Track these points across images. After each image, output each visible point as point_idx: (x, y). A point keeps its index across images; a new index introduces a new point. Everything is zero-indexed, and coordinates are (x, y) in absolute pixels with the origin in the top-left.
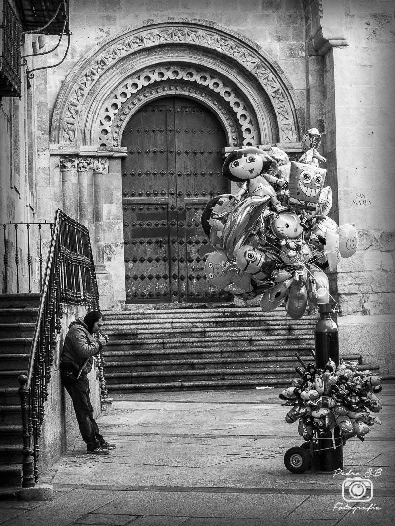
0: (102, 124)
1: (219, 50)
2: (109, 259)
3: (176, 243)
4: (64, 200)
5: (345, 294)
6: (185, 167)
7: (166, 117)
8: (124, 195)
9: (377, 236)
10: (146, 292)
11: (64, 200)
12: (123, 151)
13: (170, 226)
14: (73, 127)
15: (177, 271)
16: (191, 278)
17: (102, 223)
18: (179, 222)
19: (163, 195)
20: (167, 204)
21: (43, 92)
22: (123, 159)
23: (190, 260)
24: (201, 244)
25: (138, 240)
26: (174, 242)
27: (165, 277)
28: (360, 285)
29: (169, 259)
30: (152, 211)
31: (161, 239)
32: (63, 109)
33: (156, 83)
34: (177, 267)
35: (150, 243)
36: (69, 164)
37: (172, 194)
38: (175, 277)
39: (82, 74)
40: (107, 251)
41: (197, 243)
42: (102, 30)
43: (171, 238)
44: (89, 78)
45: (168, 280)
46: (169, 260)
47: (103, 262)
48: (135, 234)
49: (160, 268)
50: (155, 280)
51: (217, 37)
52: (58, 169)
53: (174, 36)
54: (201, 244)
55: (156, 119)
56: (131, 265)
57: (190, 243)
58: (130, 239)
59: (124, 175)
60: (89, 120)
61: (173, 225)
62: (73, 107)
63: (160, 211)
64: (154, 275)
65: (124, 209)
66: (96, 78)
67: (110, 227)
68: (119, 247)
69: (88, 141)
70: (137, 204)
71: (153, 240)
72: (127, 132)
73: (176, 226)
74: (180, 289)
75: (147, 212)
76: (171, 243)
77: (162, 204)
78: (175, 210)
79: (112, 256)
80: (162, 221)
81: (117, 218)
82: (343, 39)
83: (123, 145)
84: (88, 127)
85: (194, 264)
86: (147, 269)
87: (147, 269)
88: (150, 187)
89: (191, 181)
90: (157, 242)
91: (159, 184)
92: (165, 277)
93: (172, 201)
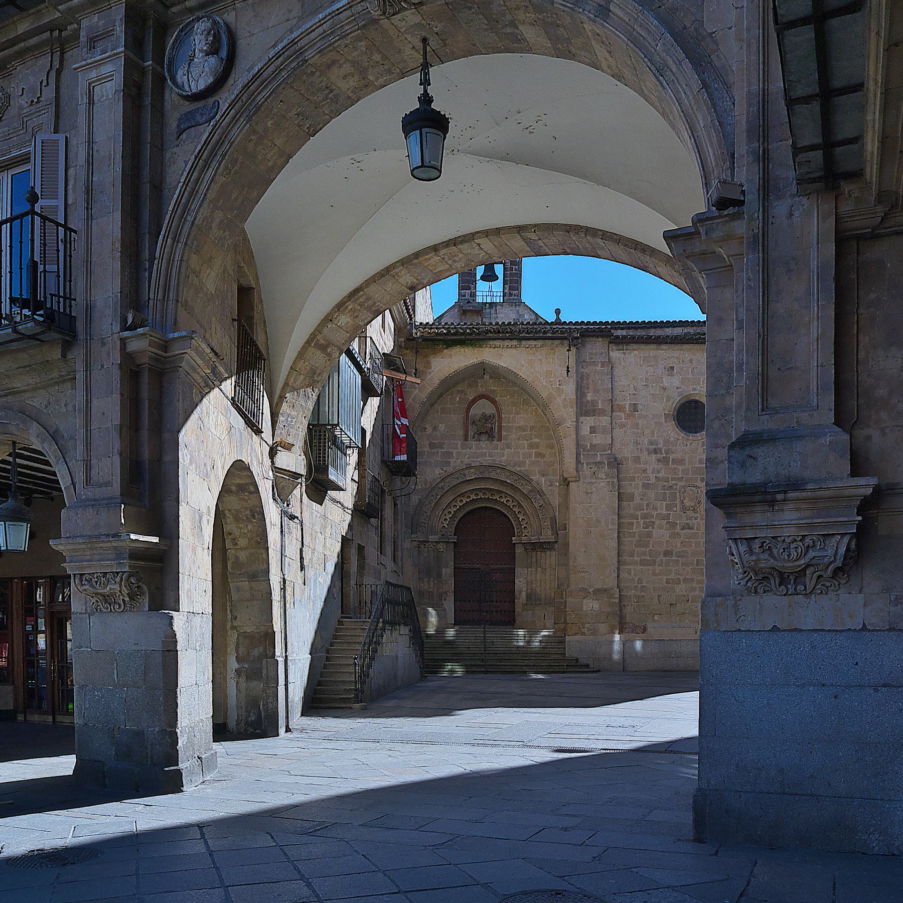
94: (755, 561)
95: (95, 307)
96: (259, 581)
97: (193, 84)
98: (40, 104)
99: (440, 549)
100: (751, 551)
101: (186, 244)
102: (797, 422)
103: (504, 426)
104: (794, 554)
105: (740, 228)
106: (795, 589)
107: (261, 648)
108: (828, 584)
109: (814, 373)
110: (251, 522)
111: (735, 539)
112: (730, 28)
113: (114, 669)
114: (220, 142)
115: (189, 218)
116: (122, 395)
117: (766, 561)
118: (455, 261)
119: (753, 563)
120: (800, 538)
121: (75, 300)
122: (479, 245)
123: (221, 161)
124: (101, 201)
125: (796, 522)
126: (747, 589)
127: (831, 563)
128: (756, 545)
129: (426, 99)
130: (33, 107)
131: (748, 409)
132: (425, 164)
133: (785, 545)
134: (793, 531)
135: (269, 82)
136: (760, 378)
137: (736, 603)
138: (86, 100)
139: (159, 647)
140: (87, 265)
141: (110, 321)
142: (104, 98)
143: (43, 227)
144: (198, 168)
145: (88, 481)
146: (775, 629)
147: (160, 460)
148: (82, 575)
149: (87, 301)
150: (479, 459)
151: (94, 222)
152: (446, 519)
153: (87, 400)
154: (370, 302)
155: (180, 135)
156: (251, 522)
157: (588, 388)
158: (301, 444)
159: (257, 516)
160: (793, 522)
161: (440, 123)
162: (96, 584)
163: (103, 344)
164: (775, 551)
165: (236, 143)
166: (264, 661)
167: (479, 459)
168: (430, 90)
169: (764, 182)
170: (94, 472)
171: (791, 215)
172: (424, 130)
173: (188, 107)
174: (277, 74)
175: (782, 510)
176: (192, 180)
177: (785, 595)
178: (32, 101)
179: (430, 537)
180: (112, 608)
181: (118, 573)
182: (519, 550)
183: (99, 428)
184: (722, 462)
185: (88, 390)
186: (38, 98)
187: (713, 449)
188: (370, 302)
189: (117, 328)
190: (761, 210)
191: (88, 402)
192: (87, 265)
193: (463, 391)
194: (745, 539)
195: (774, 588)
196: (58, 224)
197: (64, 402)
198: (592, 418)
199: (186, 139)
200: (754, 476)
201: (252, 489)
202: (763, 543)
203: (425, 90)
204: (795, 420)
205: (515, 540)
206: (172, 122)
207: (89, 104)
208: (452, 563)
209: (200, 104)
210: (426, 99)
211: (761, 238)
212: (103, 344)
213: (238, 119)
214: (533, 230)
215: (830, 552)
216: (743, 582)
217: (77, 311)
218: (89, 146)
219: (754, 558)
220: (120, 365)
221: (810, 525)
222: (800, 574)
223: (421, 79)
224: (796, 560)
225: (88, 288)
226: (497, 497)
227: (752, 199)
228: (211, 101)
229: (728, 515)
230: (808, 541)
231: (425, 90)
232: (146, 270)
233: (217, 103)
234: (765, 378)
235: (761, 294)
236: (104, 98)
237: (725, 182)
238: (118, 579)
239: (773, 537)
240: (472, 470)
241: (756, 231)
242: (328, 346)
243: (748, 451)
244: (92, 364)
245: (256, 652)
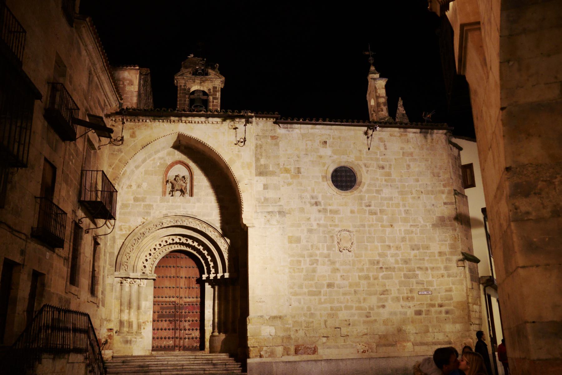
0: (143, 263)
1: (199, 228)
2: (144, 329)
3: (179, 321)
4: (121, 299)
5: (251, 347)
6: (185, 285)
7: (176, 261)
8: (154, 297)
9: (267, 319)
10: (163, 346)
11: (121, 299)
12: (155, 276)
13: (176, 313)
14: (127, 264)
15: (179, 335)
16: (185, 338)
17: (141, 311)
18: (180, 311)
19: (173, 297)
20: (175, 302)
21: (112, 247)
22: (154, 280)
23: (185, 330)
24: (191, 322)
25: (160, 319)
26: (177, 321)
27: (172, 338)
28: (258, 342)
29: (175, 329)
30: (168, 305)
31: (171, 319)
32: (123, 255)
33: (176, 243)
34: (178, 333)
35: (166, 321)
36: (124, 282)
37: (177, 297)
38: (177, 338)
39: (133, 239)
40: (144, 324)
41: (189, 321)
42: (144, 218)
43: (176, 319)
44: (136, 241)
45: (174, 339)
46: (175, 329)
47: (141, 330)
48: (159, 317)
49: (170, 334)
50: (167, 339)
51: (198, 222)
52: (119, 284)
53: (177, 222)
54: (191, 322)
55: (171, 262)
56: (156, 331)
57: (185, 321)
58: (156, 319)
59: (155, 288)
60: (136, 261)
61: (177, 312)
62: (128, 254)
63: (172, 305)
64: (167, 337)
65: (154, 304)
66: (140, 241)
67: (145, 313)
68: (149, 323)
69: (135, 271)
70: (161, 302)
71: (168, 319)
72: (158, 267)
73: (179, 313)
74: (179, 344)
75: (165, 306)
76: (176, 322)
77: (172, 302)
78: (179, 305)
79: (146, 327)
80: (172, 310)
81: (149, 308)
82: (253, 224)
83: (155, 273)
84: (136, 264)
85: (187, 332)
86: (165, 334)
87: (165, 334)
88: (167, 294)
89: (187, 291)
90: (169, 321)
91: (171, 292)
92: (172, 338)
93: (177, 300)
157: (261, 155)
167: (175, 211)
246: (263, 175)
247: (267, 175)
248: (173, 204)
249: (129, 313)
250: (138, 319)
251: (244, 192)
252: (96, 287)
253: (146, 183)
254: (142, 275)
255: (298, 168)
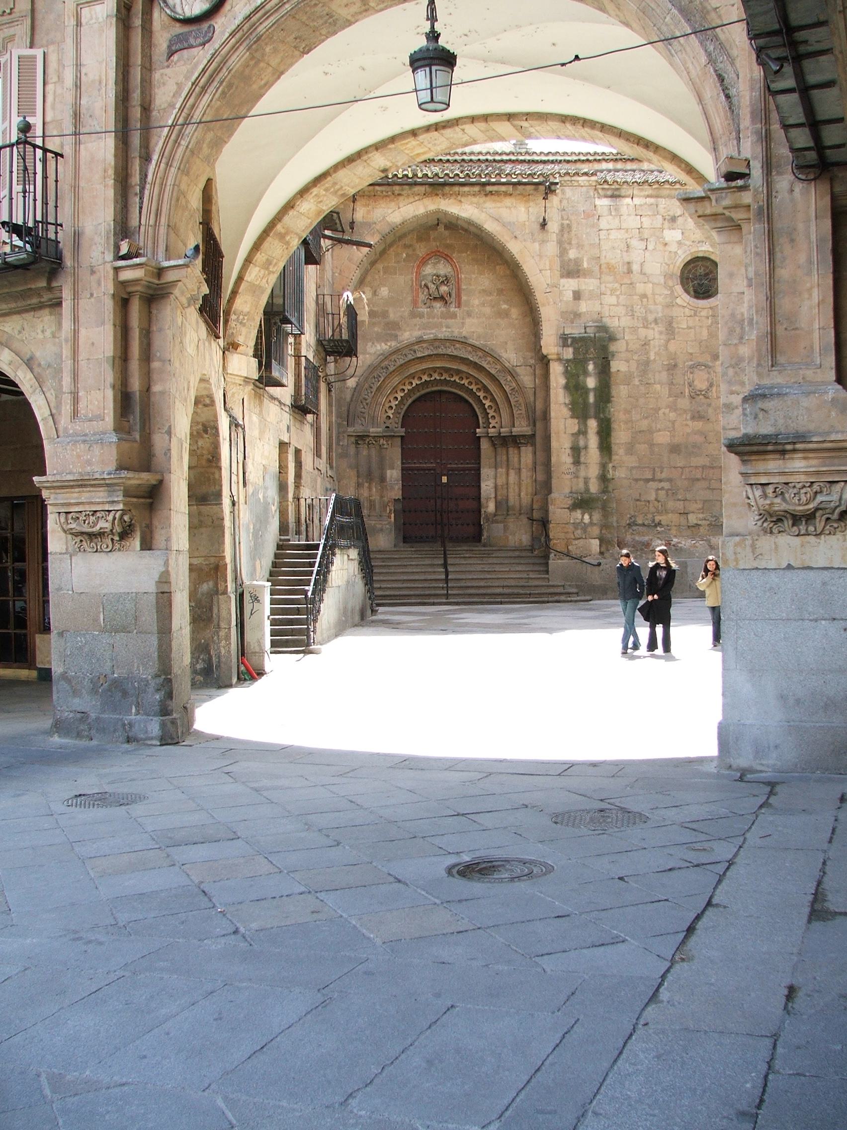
12: (402, 432)
94: (770, 505)
95: (83, 233)
96: (209, 505)
97: (186, 8)
98: (13, 16)
99: (383, 445)
100: (765, 496)
101: (179, 169)
102: (803, 378)
103: (464, 289)
104: (804, 499)
105: (747, 198)
106: (807, 530)
107: (211, 584)
108: (836, 525)
109: (816, 335)
110: (202, 437)
111: (751, 484)
112: (733, 5)
113: (99, 613)
114: (218, 70)
115: (183, 142)
116: (115, 325)
117: (779, 505)
118: (435, 145)
119: (767, 507)
120: (809, 484)
121: (61, 225)
122: (463, 130)
123: (218, 88)
124: (90, 126)
125: (805, 470)
126: (763, 530)
127: (836, 507)
128: (770, 490)
129: (433, 36)
130: (4, 18)
131: (759, 365)
132: (435, 99)
133: (795, 491)
134: (803, 478)
135: (272, 14)
136: (769, 336)
137: (753, 542)
138: (73, 22)
139: (152, 588)
140: (75, 190)
141: (101, 249)
142: (94, 21)
143: (44, 161)
144: (194, 94)
145: (75, 414)
146: (789, 567)
147: (148, 389)
148: (67, 513)
149: (74, 227)
150: (433, 331)
151: (82, 147)
152: (391, 407)
153: (74, 329)
154: (337, 187)
155: (171, 56)
156: (202, 437)
157: (570, 243)
158: (252, 343)
159: (209, 431)
160: (802, 470)
161: (448, 60)
162: (84, 523)
163: (93, 272)
164: (787, 496)
165: (234, 70)
166: (215, 598)
167: (433, 331)
168: (438, 27)
169: (767, 160)
170: (82, 405)
171: (792, 191)
172: (434, 68)
173: (179, 29)
174: (280, 7)
175: (792, 459)
176: (187, 106)
177: (797, 535)
178: (4, 12)
179: (371, 430)
180: (99, 547)
181: (109, 511)
182: (485, 445)
183: (88, 359)
184: (737, 407)
185: (76, 320)
186: (11, 9)
187: (729, 395)
188: (337, 187)
189: (109, 257)
190: (765, 185)
191: (76, 333)
192: (75, 190)
193: (411, 246)
194: (761, 484)
195: (787, 529)
196: (35, 146)
197: (42, 329)
198: (576, 280)
199: (178, 61)
200: (766, 429)
201: (207, 401)
202: (776, 488)
203: (433, 27)
204: (801, 377)
205: (480, 433)
206: (162, 40)
207: (77, 26)
208: (399, 463)
209: (193, 27)
210: (433, 36)
211: (766, 211)
212: (93, 272)
213: (238, 47)
214: (524, 118)
215: (835, 497)
216: (760, 523)
217: (64, 237)
218: (77, 69)
219: (768, 502)
220: (113, 295)
221: (818, 473)
222: (810, 517)
223: (428, 16)
224: (806, 504)
225: (76, 214)
226: (456, 378)
227: (757, 172)
228: (205, 26)
229: (744, 462)
230: (816, 487)
231: (433, 27)
232: (136, 194)
233: (212, 29)
234: (773, 336)
235: (767, 260)
236: (94, 21)
237: (731, 158)
238: (110, 518)
239: (785, 483)
240: (424, 345)
241: (762, 203)
242: (287, 233)
243: (760, 404)
244: (80, 293)
245: (205, 587)
246: (573, 277)
247: (579, 277)
248: (431, 320)
249: (370, 488)
250: (382, 497)
251: (544, 305)
252: (119, 354)
253: (387, 288)
254: (386, 432)
255: (629, 263)
